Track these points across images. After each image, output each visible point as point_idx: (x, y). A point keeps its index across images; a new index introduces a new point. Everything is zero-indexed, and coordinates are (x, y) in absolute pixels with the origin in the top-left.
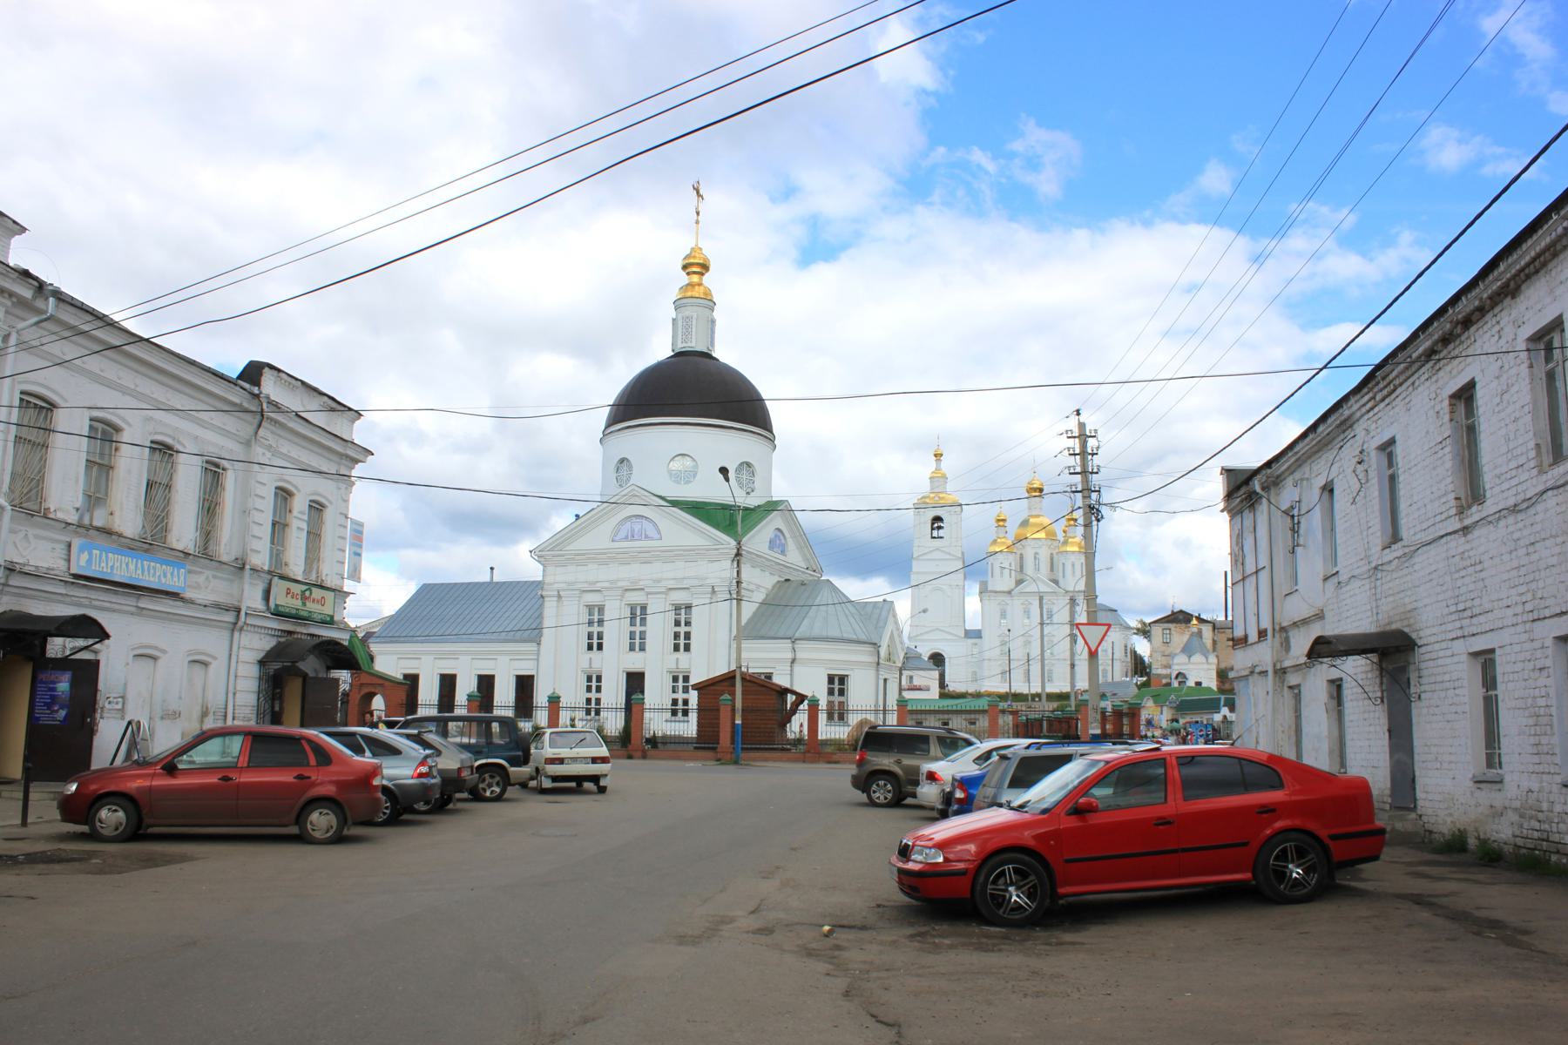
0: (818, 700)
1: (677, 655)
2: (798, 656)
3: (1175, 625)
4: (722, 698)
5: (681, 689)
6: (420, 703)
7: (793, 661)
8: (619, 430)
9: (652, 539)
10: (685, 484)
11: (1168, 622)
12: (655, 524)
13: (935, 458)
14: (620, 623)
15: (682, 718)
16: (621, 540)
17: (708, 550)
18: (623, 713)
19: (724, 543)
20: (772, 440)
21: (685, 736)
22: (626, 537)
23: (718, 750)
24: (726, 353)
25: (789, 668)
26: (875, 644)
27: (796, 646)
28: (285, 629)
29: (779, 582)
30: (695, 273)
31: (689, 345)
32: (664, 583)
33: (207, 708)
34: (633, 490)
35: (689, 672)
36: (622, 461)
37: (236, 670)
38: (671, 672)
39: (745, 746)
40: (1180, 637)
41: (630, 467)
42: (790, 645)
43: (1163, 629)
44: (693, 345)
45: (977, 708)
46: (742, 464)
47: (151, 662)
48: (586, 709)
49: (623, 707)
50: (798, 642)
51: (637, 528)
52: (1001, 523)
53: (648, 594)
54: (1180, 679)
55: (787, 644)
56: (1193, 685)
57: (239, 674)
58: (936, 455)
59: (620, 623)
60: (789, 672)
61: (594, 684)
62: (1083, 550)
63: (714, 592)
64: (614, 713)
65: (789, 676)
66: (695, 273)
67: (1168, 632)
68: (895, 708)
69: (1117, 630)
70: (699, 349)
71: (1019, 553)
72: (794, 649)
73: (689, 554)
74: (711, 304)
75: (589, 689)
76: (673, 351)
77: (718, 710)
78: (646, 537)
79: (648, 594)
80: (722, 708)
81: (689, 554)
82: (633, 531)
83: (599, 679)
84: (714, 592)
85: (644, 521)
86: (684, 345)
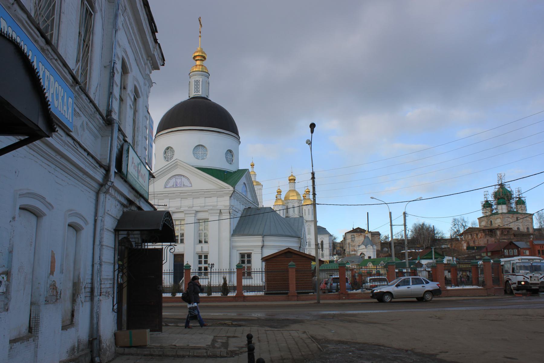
0: (190, 266)
1: (200, 245)
2: (265, 244)
3: (356, 233)
4: (290, 264)
5: (203, 262)
6: (163, 272)
7: (263, 247)
8: (166, 133)
9: (187, 186)
10: (201, 159)
11: (353, 232)
12: (188, 179)
13: (251, 166)
14: (283, 211)
15: (204, 277)
16: (170, 187)
17: (217, 191)
18: (173, 275)
19: (226, 188)
20: (238, 138)
21: (253, 285)
22: (173, 186)
23: (289, 294)
24: (214, 98)
25: (261, 250)
26: (299, 238)
27: (264, 239)
28: (128, 196)
29: (245, 209)
30: (198, 60)
31: (198, 93)
32: (194, 208)
33: (79, 279)
34: (177, 162)
35: (208, 253)
36: (168, 148)
37: (101, 238)
38: (198, 254)
39: (299, 291)
40: (360, 239)
41: (173, 151)
42: (262, 239)
43: (351, 235)
44: (200, 93)
45: (333, 268)
46: (228, 150)
47: (33, 219)
48: (199, 272)
49: (173, 272)
50: (265, 237)
51: (179, 181)
52: (279, 193)
53: (185, 214)
54: (362, 256)
55: (260, 238)
56: (368, 258)
57: (104, 243)
58: (251, 165)
59: (283, 211)
60: (260, 252)
61: (203, 260)
62: (312, 203)
63: (220, 212)
64: (261, 274)
65: (261, 254)
66: (198, 60)
67: (353, 236)
68: (235, 270)
69: (327, 236)
70: (203, 96)
71: (286, 205)
72: (263, 240)
73: (207, 194)
74: (208, 75)
75: (200, 262)
76: (189, 97)
77: (288, 271)
78: (184, 185)
79: (185, 214)
80: (290, 270)
81: (207, 194)
82: (176, 182)
83: (206, 257)
84: (220, 212)
85: (182, 177)
86: (196, 94)
